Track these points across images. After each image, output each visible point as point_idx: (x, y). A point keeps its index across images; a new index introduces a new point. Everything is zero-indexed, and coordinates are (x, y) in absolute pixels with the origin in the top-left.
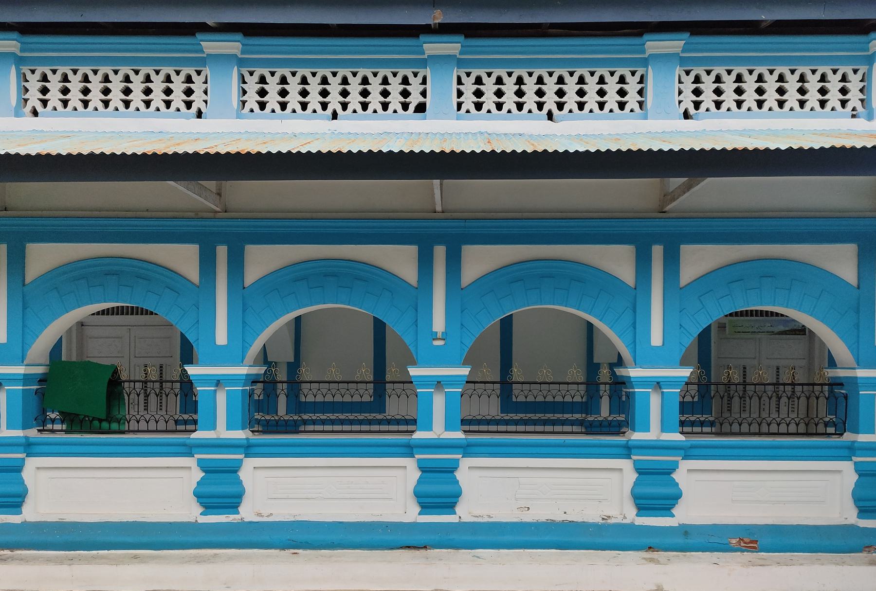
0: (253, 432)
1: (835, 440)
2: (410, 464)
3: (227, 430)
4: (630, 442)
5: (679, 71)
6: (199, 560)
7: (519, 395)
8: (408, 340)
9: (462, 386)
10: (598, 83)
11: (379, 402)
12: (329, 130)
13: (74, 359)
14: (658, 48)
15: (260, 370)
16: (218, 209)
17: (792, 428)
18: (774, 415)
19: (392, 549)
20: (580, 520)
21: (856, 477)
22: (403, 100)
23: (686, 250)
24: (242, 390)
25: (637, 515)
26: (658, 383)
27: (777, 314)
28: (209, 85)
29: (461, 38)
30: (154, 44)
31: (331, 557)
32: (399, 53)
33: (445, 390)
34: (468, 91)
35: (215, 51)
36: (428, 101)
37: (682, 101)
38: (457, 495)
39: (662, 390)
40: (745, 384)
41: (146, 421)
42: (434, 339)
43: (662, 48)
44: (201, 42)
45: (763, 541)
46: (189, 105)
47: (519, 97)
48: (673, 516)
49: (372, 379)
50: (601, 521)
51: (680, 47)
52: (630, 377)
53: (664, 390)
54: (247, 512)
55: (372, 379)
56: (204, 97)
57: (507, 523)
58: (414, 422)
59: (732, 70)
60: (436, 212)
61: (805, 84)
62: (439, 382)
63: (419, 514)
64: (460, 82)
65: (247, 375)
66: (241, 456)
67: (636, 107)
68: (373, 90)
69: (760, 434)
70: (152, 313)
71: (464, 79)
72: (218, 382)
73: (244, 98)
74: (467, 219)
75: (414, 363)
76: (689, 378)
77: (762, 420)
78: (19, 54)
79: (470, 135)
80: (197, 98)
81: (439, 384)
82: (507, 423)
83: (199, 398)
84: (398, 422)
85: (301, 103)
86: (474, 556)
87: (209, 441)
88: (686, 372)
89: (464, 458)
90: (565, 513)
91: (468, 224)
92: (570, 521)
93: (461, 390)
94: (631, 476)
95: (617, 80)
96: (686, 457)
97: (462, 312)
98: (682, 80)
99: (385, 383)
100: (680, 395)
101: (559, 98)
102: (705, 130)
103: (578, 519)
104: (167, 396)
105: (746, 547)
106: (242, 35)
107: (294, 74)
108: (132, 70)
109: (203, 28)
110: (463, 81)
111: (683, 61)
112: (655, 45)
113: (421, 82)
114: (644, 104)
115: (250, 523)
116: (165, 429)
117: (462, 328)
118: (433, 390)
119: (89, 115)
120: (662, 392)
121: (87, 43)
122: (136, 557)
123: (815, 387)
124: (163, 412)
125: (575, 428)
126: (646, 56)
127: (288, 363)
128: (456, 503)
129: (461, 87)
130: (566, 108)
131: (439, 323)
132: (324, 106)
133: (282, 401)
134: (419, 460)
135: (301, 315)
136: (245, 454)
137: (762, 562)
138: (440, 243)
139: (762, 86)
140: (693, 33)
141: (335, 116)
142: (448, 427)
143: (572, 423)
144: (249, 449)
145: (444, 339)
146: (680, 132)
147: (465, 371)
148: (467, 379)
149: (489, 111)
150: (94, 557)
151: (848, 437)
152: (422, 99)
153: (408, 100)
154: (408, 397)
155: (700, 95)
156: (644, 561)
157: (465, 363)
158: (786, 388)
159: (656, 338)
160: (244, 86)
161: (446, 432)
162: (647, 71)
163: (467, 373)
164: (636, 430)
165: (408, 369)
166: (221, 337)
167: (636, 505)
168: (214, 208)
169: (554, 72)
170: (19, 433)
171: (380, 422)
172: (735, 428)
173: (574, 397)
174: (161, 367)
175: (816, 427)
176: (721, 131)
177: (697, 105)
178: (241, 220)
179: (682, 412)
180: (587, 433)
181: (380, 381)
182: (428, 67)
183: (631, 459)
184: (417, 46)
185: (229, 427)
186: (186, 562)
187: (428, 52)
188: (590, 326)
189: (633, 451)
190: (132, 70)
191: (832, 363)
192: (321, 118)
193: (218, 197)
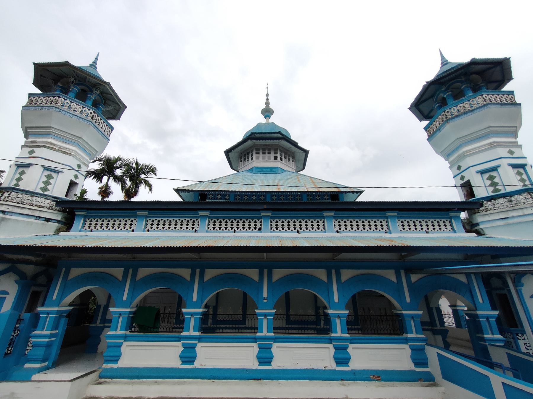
1: (401, 337)
2: (255, 345)
5: (333, 220)
6: (179, 384)
7: (292, 318)
10: (311, 223)
11: (244, 321)
13: (142, 306)
17: (389, 332)
19: (248, 380)
20: (316, 368)
21: (258, 349)
22: (249, 227)
24: (55, 316)
25: (336, 366)
26: (338, 315)
31: (226, 383)
38: (272, 358)
40: (164, 314)
42: (264, 300)
45: (383, 377)
46: (193, 228)
53: (341, 318)
54: (197, 364)
56: (198, 226)
62: (265, 315)
64: (271, 222)
66: (197, 342)
67: (323, 229)
72: (192, 315)
75: (257, 308)
76: (275, 313)
80: (196, 227)
81: (265, 315)
82: (288, 329)
85: (306, 228)
86: (278, 383)
88: (347, 312)
93: (273, 318)
94: (333, 351)
110: (272, 222)
111: (334, 218)
115: (198, 368)
122: (156, 382)
123: (236, 315)
124: (169, 325)
125: (313, 332)
126: (261, 216)
128: (272, 361)
129: (272, 224)
131: (265, 295)
134: (258, 344)
137: (382, 385)
141: (235, 231)
143: (311, 329)
144: (200, 339)
145: (267, 300)
147: (274, 311)
150: (144, 382)
151: (405, 335)
152: (260, 227)
156: (340, 385)
157: (274, 308)
159: (336, 300)
162: (325, 220)
164: (333, 332)
166: (195, 299)
167: (258, 361)
170: (123, 332)
172: (369, 332)
177: (340, 229)
179: (347, 325)
180: (317, 334)
181: (245, 315)
184: (135, 212)
186: (174, 385)
188: (316, 296)
189: (332, 340)
191: (395, 309)
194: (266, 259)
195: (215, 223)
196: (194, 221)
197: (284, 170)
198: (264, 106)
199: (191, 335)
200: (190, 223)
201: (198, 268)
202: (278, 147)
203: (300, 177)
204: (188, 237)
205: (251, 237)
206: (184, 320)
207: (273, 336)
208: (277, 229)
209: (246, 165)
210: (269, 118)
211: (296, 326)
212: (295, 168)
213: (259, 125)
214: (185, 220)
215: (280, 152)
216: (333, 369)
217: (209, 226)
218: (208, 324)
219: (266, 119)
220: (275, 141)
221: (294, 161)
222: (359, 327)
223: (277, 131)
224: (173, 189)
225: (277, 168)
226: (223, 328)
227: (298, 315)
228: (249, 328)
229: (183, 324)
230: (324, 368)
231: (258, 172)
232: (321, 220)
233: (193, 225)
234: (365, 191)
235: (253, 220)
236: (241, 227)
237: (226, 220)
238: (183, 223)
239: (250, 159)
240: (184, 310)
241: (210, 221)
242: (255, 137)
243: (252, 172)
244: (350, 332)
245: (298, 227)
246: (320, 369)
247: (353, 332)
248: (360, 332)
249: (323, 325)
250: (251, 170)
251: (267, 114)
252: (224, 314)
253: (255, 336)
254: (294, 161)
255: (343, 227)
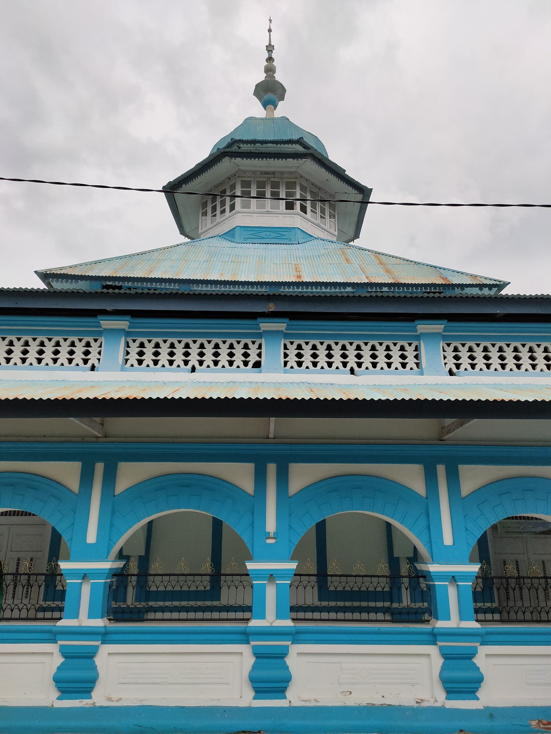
0: (110, 620)
2: (245, 649)
3: (88, 619)
4: (435, 630)
5: (442, 344)
7: (334, 584)
8: (246, 539)
9: (291, 579)
12: (190, 379)
14: (425, 329)
15: (120, 564)
16: (100, 435)
18: (519, 604)
20: (397, 704)
23: (462, 468)
26: (453, 577)
27: (536, 519)
28: (102, 348)
29: (287, 320)
30: (56, 321)
32: (206, 328)
33: (277, 582)
34: (292, 354)
35: (118, 327)
36: (263, 360)
37: (447, 363)
38: (288, 680)
39: (457, 583)
40: (16, 574)
41: (19, 609)
42: (267, 538)
43: (429, 329)
44: (100, 321)
46: (86, 361)
47: (329, 359)
48: (478, 699)
49: (316, 573)
50: (416, 705)
51: (441, 329)
52: (429, 572)
53: (459, 583)
55: (316, 573)
56: (98, 356)
57: (332, 707)
58: (249, 609)
59: (465, 344)
60: (268, 438)
61: (534, 354)
62: (271, 575)
63: (58, 699)
64: (285, 348)
65: (110, 569)
66: (98, 643)
67: (414, 366)
68: (222, 352)
69: (539, 621)
70: (34, 515)
71: (289, 345)
72: (85, 576)
73: (127, 357)
74: (293, 444)
75: (250, 558)
76: (296, 570)
77: (541, 609)
78: (127, 330)
79: (283, 384)
80: (93, 358)
81: (271, 576)
83: (68, 589)
84: (235, 609)
87: (72, 629)
89: (293, 645)
90: (383, 697)
91: (293, 447)
92: (388, 705)
93: (289, 582)
94: (438, 662)
95: (311, 348)
96: (483, 643)
97: (290, 516)
98: (445, 349)
99: (148, 576)
100: (472, 587)
101: (358, 359)
102: (466, 383)
103: (394, 702)
104: (7, 587)
105: (545, 728)
106: (130, 317)
107: (224, 342)
108: (47, 338)
109: (104, 312)
110: (288, 347)
111: (444, 338)
112: (423, 327)
113: (257, 347)
114: (420, 364)
115: (101, 707)
116: (51, 617)
117: (290, 529)
118: (266, 582)
119: (10, 369)
120: (277, 584)
121: (17, 321)
123: (534, 580)
125: (380, 616)
126: (261, 331)
127: (140, 556)
128: (287, 687)
130: (364, 366)
131: (271, 525)
132: (186, 363)
133: (131, 593)
134: (254, 647)
135: (152, 520)
136: (102, 641)
138: (272, 462)
139: (503, 355)
140: (449, 321)
141: (193, 369)
142: (279, 616)
145: (275, 538)
146: (449, 384)
147: (293, 566)
148: (295, 572)
149: (238, 367)
152: (258, 359)
153: (248, 359)
154: (244, 588)
155: (459, 359)
157: (293, 559)
158: (153, 579)
159: (448, 540)
160: (128, 349)
161: (277, 620)
162: (420, 344)
163: (295, 567)
164: (439, 619)
165: (246, 564)
166: (92, 537)
168: (98, 435)
169: (256, 341)
171: (212, 609)
172: (528, 616)
173: (306, 587)
174: (19, 560)
175: (540, 615)
176: (478, 384)
177: (458, 366)
178: (117, 444)
179: (475, 600)
180: (393, 621)
182: (263, 338)
183: (437, 645)
185: (91, 616)
187: (420, 331)
190: (47, 338)
192: (184, 371)
193: (101, 426)
194: (274, 438)
195: (144, 350)
196: (88, 345)
197: (312, 236)
198: (261, 77)
199: (83, 625)
200: (79, 349)
201: (100, 461)
202: (297, 178)
203: (348, 251)
204: (72, 382)
205: (236, 382)
206: (64, 592)
207: (478, 628)
208: (300, 364)
209: (218, 223)
210: (272, 107)
211: (341, 604)
212: (336, 233)
213: (249, 121)
214: (65, 340)
215: (301, 190)
216: (438, 704)
217: (127, 357)
218: (125, 601)
219: (265, 110)
220: (290, 162)
221: (334, 218)
222: (495, 605)
223: (295, 137)
224: (36, 272)
225: (292, 230)
226: (163, 610)
227: (351, 576)
228: (228, 609)
229: (63, 599)
230: (417, 702)
231: (245, 241)
232: (410, 345)
233: (87, 353)
234: (510, 283)
235: (239, 342)
236: (209, 358)
237: (170, 340)
238: (59, 348)
239: (227, 208)
240: (64, 565)
241: (131, 343)
242: (239, 151)
243: (232, 239)
244: (481, 616)
245: (352, 361)
246: (406, 705)
247: (489, 616)
248: (497, 616)
249: (406, 601)
250: (230, 235)
251: (270, 96)
252: (167, 575)
253: (247, 627)
254: (334, 218)
255: (465, 362)
